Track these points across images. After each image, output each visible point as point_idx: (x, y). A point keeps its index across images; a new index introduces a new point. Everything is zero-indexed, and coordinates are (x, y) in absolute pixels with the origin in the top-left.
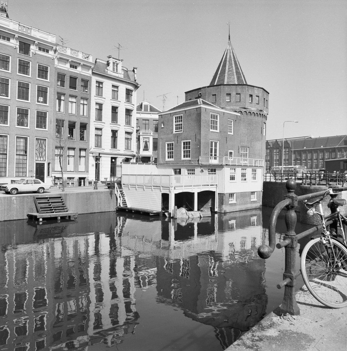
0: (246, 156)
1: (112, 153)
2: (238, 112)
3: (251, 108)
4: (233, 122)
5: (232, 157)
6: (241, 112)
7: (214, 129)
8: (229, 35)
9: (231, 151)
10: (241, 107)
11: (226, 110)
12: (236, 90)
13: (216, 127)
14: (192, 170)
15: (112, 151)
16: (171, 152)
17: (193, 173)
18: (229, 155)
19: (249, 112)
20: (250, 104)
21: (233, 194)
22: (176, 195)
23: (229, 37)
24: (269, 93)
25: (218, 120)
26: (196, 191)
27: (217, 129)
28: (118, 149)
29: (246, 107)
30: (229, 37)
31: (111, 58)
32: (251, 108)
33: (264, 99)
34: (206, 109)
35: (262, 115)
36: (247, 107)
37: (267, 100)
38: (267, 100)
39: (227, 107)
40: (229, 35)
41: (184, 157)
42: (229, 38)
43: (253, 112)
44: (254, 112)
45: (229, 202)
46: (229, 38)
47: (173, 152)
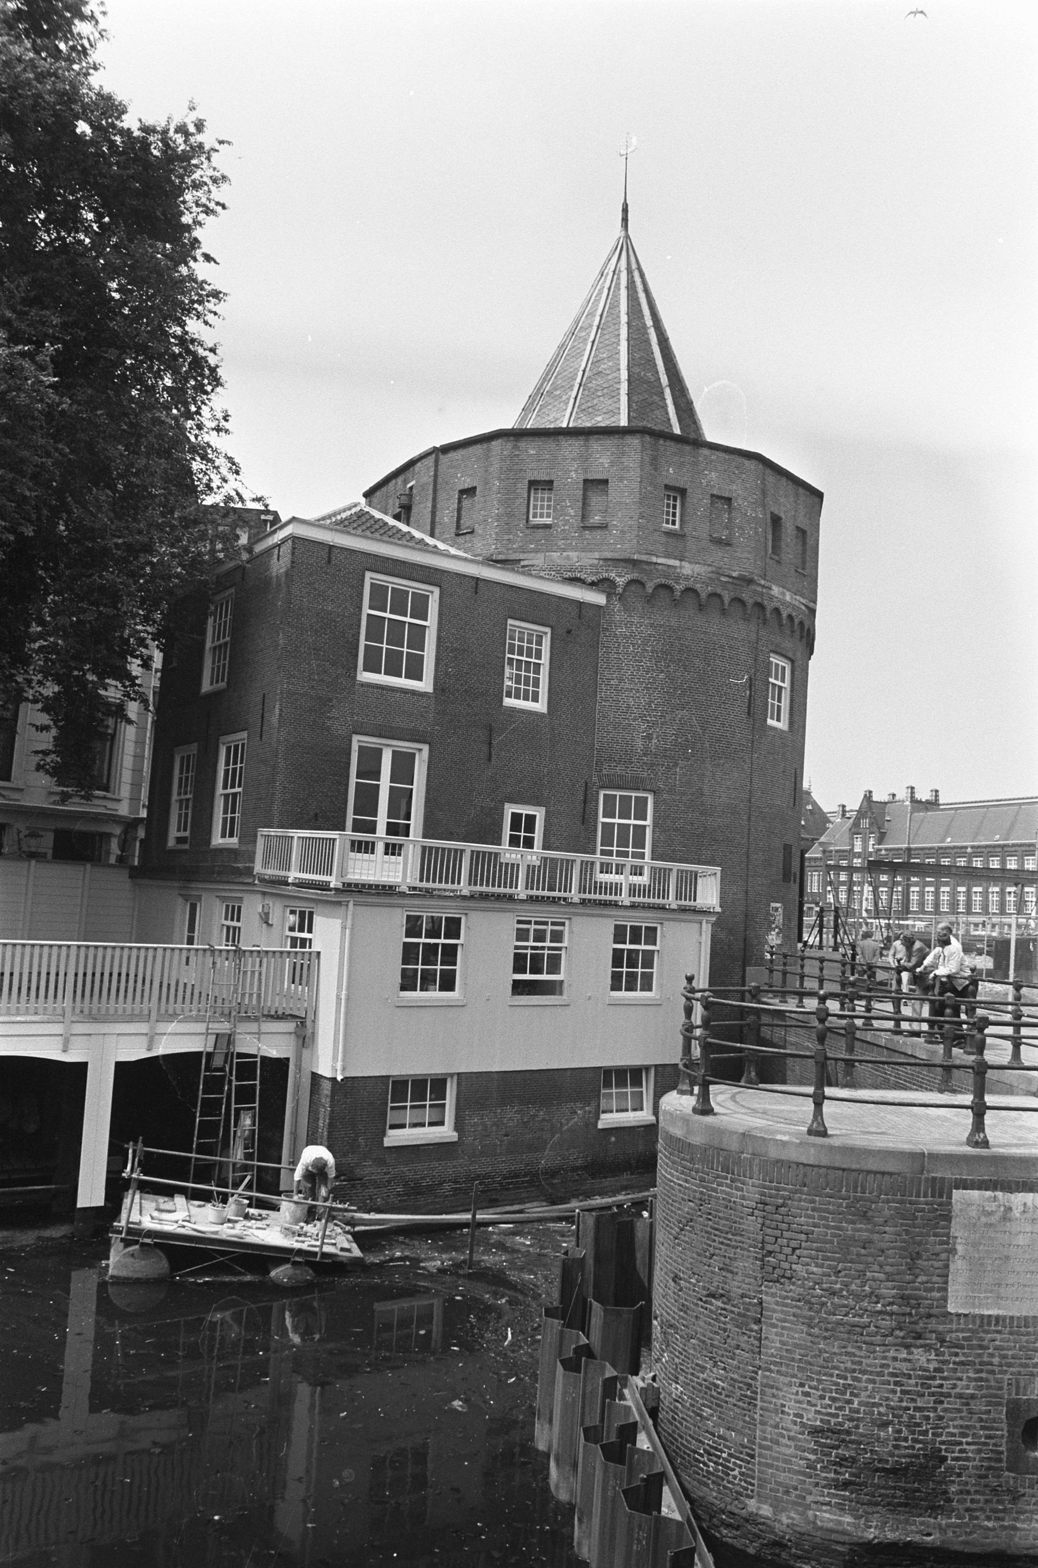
0: (640, 843)
2: (593, 584)
4: (546, 642)
5: (638, 862)
6: (612, 583)
9: (524, 810)
10: (609, 555)
11: (527, 571)
12: (584, 459)
14: (435, 922)
18: (507, 832)
20: (664, 539)
21: (444, 1081)
22: (122, 1069)
23: (625, 210)
24: (820, 495)
25: (431, 622)
27: (415, 673)
30: (625, 210)
34: (481, 585)
35: (760, 606)
39: (526, 556)
42: (625, 220)
43: (690, 584)
44: (698, 586)
45: (603, 1116)
46: (625, 220)
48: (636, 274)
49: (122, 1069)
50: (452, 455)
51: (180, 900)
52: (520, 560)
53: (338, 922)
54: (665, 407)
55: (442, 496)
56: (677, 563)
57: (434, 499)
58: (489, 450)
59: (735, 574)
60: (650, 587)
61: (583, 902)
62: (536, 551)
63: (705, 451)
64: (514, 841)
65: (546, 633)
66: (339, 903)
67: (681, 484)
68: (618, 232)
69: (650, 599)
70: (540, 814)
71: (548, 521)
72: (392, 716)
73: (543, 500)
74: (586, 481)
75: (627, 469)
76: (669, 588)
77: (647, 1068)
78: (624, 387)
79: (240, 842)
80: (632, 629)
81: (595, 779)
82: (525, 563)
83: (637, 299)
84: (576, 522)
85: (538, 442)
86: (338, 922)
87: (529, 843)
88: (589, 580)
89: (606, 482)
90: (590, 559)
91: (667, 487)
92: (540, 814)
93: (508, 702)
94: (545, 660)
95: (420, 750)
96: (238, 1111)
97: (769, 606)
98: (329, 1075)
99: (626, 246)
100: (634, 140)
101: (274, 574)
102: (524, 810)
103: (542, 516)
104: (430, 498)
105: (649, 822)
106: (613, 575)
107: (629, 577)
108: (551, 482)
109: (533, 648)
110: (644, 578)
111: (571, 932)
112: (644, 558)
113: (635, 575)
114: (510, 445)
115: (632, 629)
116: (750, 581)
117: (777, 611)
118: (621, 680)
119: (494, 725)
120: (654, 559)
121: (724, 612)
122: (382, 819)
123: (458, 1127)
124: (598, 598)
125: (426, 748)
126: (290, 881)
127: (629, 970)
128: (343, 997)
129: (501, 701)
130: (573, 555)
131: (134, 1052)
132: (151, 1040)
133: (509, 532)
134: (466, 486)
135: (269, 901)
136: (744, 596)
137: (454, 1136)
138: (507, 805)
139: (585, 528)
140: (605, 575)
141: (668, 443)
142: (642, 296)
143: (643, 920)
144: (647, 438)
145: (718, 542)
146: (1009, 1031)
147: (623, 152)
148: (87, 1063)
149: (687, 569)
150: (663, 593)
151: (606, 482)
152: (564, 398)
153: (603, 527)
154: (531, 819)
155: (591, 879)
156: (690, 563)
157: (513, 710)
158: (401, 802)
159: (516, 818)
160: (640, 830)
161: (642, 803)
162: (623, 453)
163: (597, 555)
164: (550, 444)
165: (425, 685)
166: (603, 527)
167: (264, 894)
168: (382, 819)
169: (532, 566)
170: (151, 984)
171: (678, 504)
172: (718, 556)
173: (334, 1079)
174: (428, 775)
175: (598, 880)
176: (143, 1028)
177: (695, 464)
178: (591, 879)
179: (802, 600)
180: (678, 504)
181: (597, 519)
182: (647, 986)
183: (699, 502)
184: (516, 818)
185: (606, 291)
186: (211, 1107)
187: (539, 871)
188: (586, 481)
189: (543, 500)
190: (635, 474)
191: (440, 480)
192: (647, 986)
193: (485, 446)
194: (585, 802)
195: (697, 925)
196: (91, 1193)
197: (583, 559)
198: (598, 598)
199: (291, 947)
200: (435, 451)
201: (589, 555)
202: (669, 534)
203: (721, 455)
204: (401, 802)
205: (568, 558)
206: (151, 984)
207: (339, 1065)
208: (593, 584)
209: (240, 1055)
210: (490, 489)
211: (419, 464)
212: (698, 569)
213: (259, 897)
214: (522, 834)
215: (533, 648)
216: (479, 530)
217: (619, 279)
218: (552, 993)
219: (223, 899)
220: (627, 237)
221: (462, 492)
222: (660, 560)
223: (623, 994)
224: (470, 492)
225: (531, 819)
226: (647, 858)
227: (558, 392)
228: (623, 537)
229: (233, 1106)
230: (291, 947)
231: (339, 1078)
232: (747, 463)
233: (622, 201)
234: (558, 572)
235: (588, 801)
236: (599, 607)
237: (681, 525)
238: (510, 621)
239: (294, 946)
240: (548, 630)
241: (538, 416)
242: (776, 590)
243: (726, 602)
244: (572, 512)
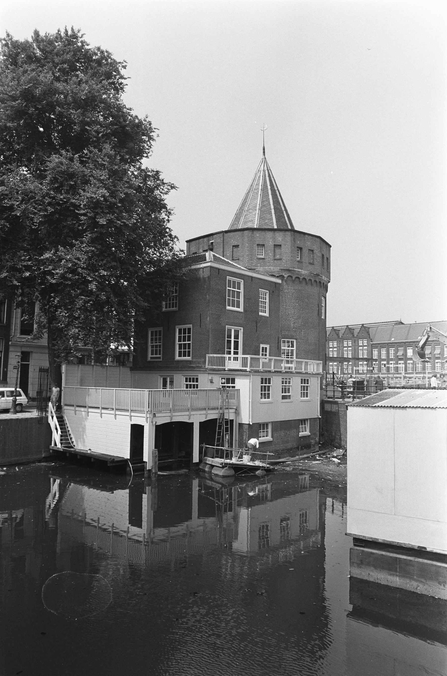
0: (292, 355)
2: (278, 277)
7: (233, 306)
9: (265, 346)
10: (282, 268)
12: (274, 238)
13: (238, 302)
19: (297, 277)
22: (201, 423)
23: (264, 149)
24: (330, 246)
25: (242, 290)
26: (197, 419)
27: (265, 313)
30: (264, 149)
35: (320, 282)
37: (327, 258)
38: (327, 258)
41: (180, 356)
42: (264, 152)
44: (306, 277)
46: (264, 152)
48: (270, 171)
49: (201, 423)
50: (229, 234)
51: (159, 377)
53: (248, 381)
54: (284, 217)
55: (226, 247)
56: (300, 270)
57: (223, 248)
58: (243, 234)
59: (315, 273)
61: (275, 372)
62: (261, 266)
63: (307, 236)
64: (263, 355)
66: (248, 375)
67: (300, 246)
68: (262, 157)
69: (293, 281)
70: (268, 346)
71: (263, 257)
72: (234, 318)
73: (260, 250)
74: (274, 245)
75: (287, 242)
77: (307, 420)
78: (273, 211)
79: (192, 358)
80: (289, 290)
81: (280, 336)
83: (272, 182)
84: (272, 258)
85: (260, 232)
86: (248, 381)
87: (266, 355)
88: (277, 276)
89: (281, 245)
90: (277, 269)
91: (298, 247)
92: (268, 346)
93: (260, 314)
94: (267, 301)
95: (240, 329)
96: (226, 434)
97: (322, 282)
98: (248, 423)
99: (265, 161)
100: (266, 126)
101: (201, 276)
102: (265, 346)
103: (260, 255)
104: (222, 247)
105: (295, 348)
107: (288, 275)
108: (264, 245)
109: (265, 297)
110: (292, 275)
111: (292, 381)
112: (292, 269)
113: (290, 274)
114: (251, 233)
115: (289, 290)
116: (318, 275)
117: (323, 283)
118: (286, 306)
119: (258, 320)
120: (295, 269)
121: (312, 284)
122: (232, 350)
123: (272, 437)
124: (279, 281)
125: (242, 328)
126: (226, 369)
127: (305, 391)
128: (251, 401)
129: (226, 308)
130: (272, 268)
131: (203, 420)
132: (206, 415)
133: (252, 260)
134: (235, 245)
135: (213, 376)
136: (317, 280)
137: (271, 439)
138: (261, 345)
139: (275, 260)
140: (281, 274)
141: (298, 234)
142: (272, 179)
143: (267, 376)
144: (292, 233)
145: (310, 263)
147: (263, 129)
148: (193, 423)
149: (303, 272)
150: (297, 279)
151: (281, 245)
152: (254, 213)
153: (280, 259)
154: (266, 348)
157: (261, 316)
158: (236, 343)
159: (263, 348)
161: (292, 343)
162: (285, 237)
163: (279, 268)
164: (263, 233)
165: (241, 309)
166: (280, 259)
167: (209, 373)
168: (232, 350)
171: (299, 252)
172: (310, 267)
173: (249, 424)
174: (243, 337)
176: (187, 413)
177: (305, 240)
180: (299, 252)
181: (278, 257)
182: (269, 398)
183: (305, 251)
184: (263, 348)
185: (261, 177)
186: (219, 434)
188: (274, 245)
189: (260, 250)
190: (289, 244)
191: (225, 241)
192: (269, 398)
193: (242, 232)
194: (278, 343)
196: (196, 459)
197: (275, 269)
198: (279, 281)
199: (186, 388)
200: (222, 232)
201: (276, 268)
202: (298, 261)
203: (310, 237)
204: (236, 343)
205: (270, 269)
207: (250, 420)
208: (278, 277)
209: (226, 419)
210: (244, 246)
211: (215, 236)
212: (306, 272)
213: (207, 375)
215: (265, 297)
216: (241, 259)
217: (265, 173)
218: (287, 399)
219: (161, 376)
220: (265, 158)
221: (233, 246)
222: (297, 270)
223: (263, 400)
224: (237, 246)
226: (268, 356)
227: (251, 211)
228: (286, 263)
229: (225, 433)
230: (186, 388)
231: (251, 423)
232: (317, 239)
234: (267, 273)
235: (279, 343)
236: (279, 284)
237: (300, 259)
238: (260, 289)
239: (187, 388)
240: (268, 291)
241: (244, 218)
244: (270, 254)
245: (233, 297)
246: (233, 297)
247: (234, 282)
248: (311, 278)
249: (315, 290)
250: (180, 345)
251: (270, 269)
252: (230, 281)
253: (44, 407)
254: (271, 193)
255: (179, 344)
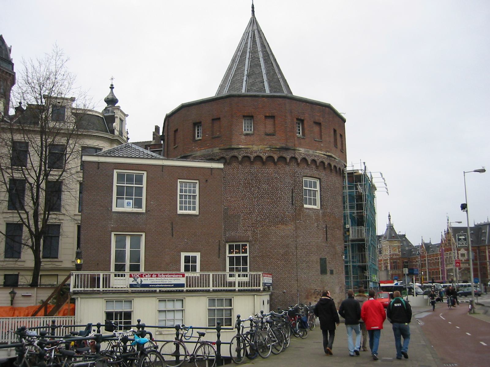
1: (6, 266)
3: (250, 146)
4: (197, 185)
7: (310, 204)
8: (253, 5)
13: (315, 200)
15: (5, 264)
16: (238, 258)
17: (122, 276)
19: (244, 157)
23: (253, 7)
28: (59, 259)
29: (233, 147)
30: (253, 7)
31: (28, 80)
32: (250, 146)
33: (335, 131)
36: (236, 147)
37: (341, 136)
40: (253, 5)
42: (253, 11)
44: (261, 155)
46: (253, 11)
47: (245, 258)
52: (191, 155)
59: (278, 147)
60: (240, 158)
61: (239, 291)
65: (197, 183)
76: (249, 157)
82: (194, 156)
92: (198, 255)
106: (225, 155)
117: (340, 169)
120: (240, 147)
146: (73, 328)
149: (255, 148)
150: (293, 160)
155: (224, 280)
156: (256, 145)
160: (245, 258)
169: (196, 156)
170: (2, 336)
175: (228, 281)
178: (224, 280)
179: (320, 152)
185: (250, 39)
187: (201, 279)
195: (253, 296)
206: (2, 336)
208: (218, 160)
214: (191, 264)
225: (194, 259)
233: (252, 4)
240: (197, 181)
242: (302, 150)
243: (299, 160)
245: (310, 195)
246: (310, 195)
247: (310, 182)
248: (272, 155)
249: (100, 164)
250: (231, 258)
251: (208, 151)
252: (306, 181)
253: (141, 329)
254: (255, 52)
255: (230, 257)
